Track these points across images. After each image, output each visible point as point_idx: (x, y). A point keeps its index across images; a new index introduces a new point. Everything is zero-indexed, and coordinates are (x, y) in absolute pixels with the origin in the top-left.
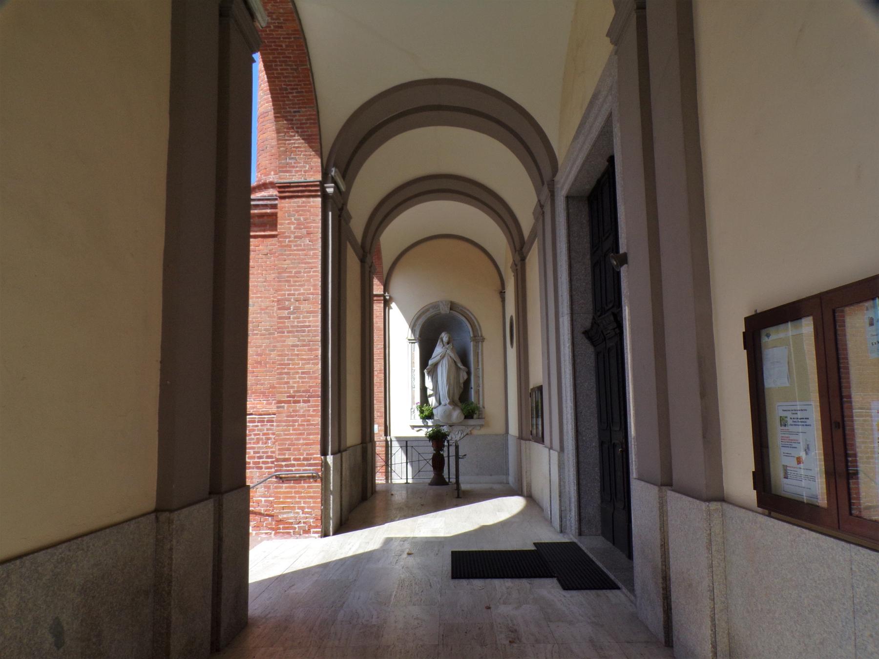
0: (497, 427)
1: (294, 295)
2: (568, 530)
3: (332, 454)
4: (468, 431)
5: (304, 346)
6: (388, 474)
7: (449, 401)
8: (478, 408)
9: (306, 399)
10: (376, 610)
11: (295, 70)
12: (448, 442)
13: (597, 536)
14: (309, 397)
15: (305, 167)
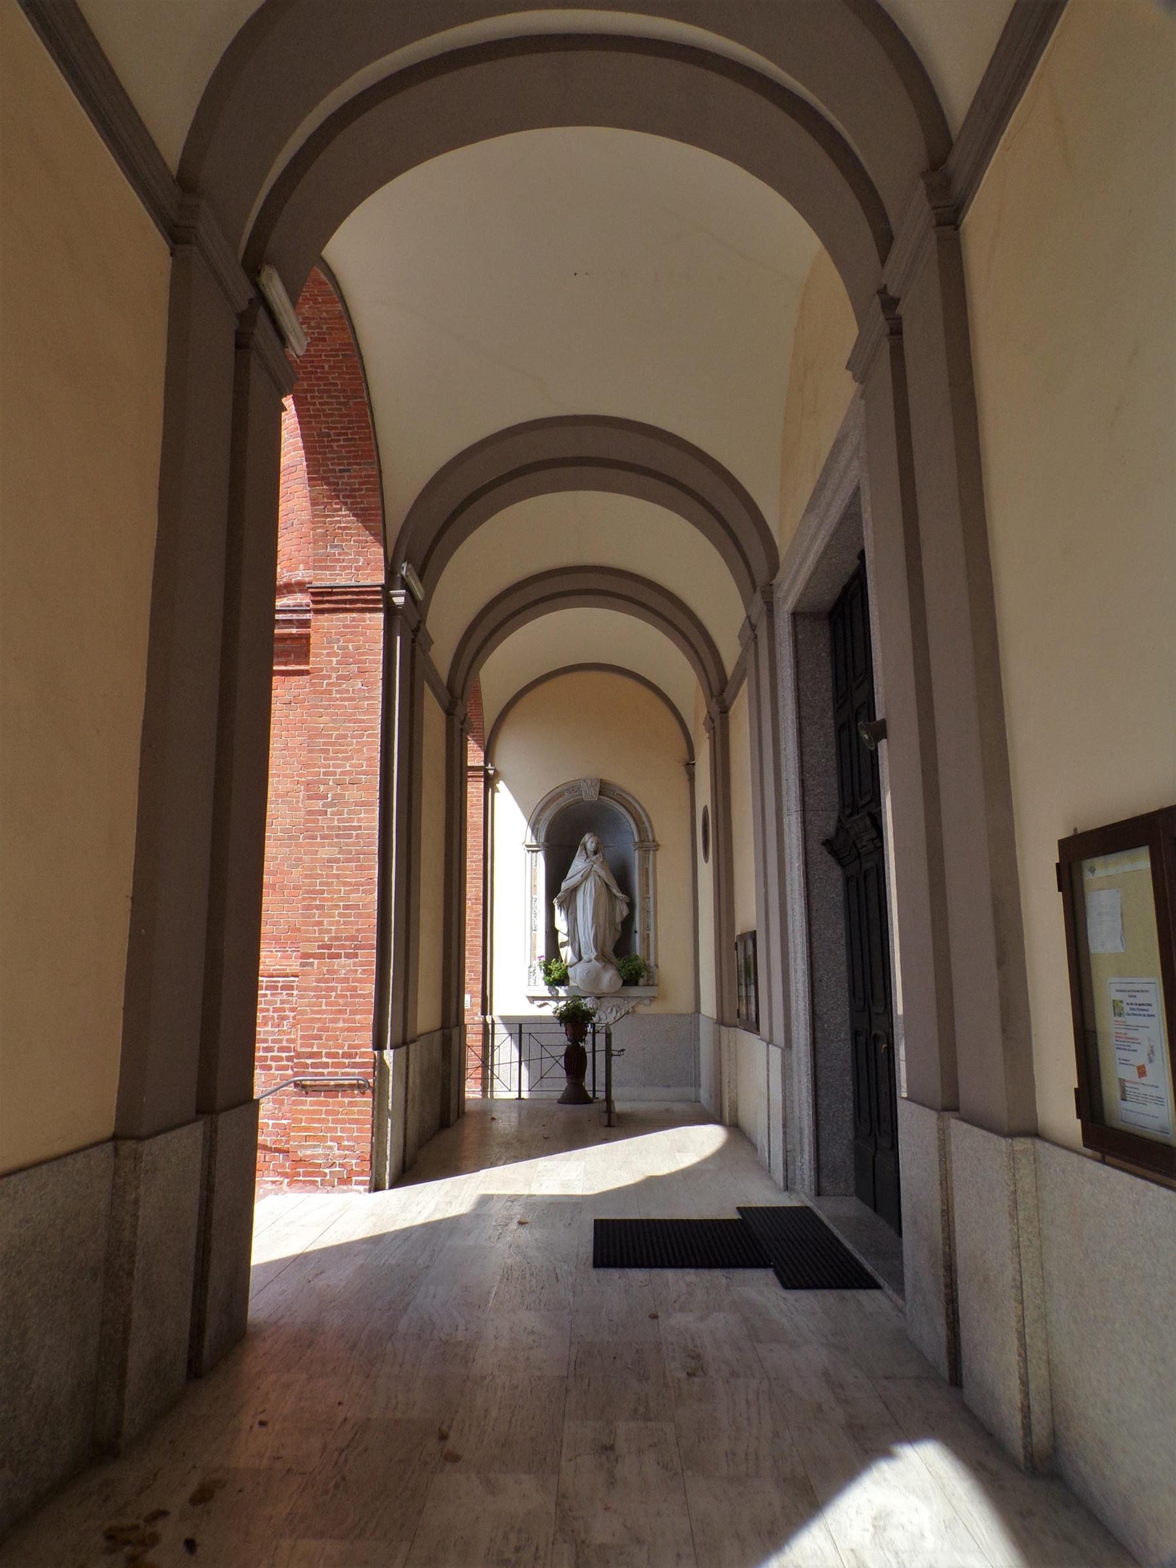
0: (680, 1003)
1: (334, 774)
2: (798, 1187)
3: (391, 1048)
4: (628, 1006)
5: (348, 860)
6: (486, 1082)
7: (595, 954)
8: (647, 968)
9: (351, 951)
10: (464, 1317)
11: (344, 404)
12: (594, 1026)
13: (847, 1196)
14: (356, 948)
15: (357, 561)
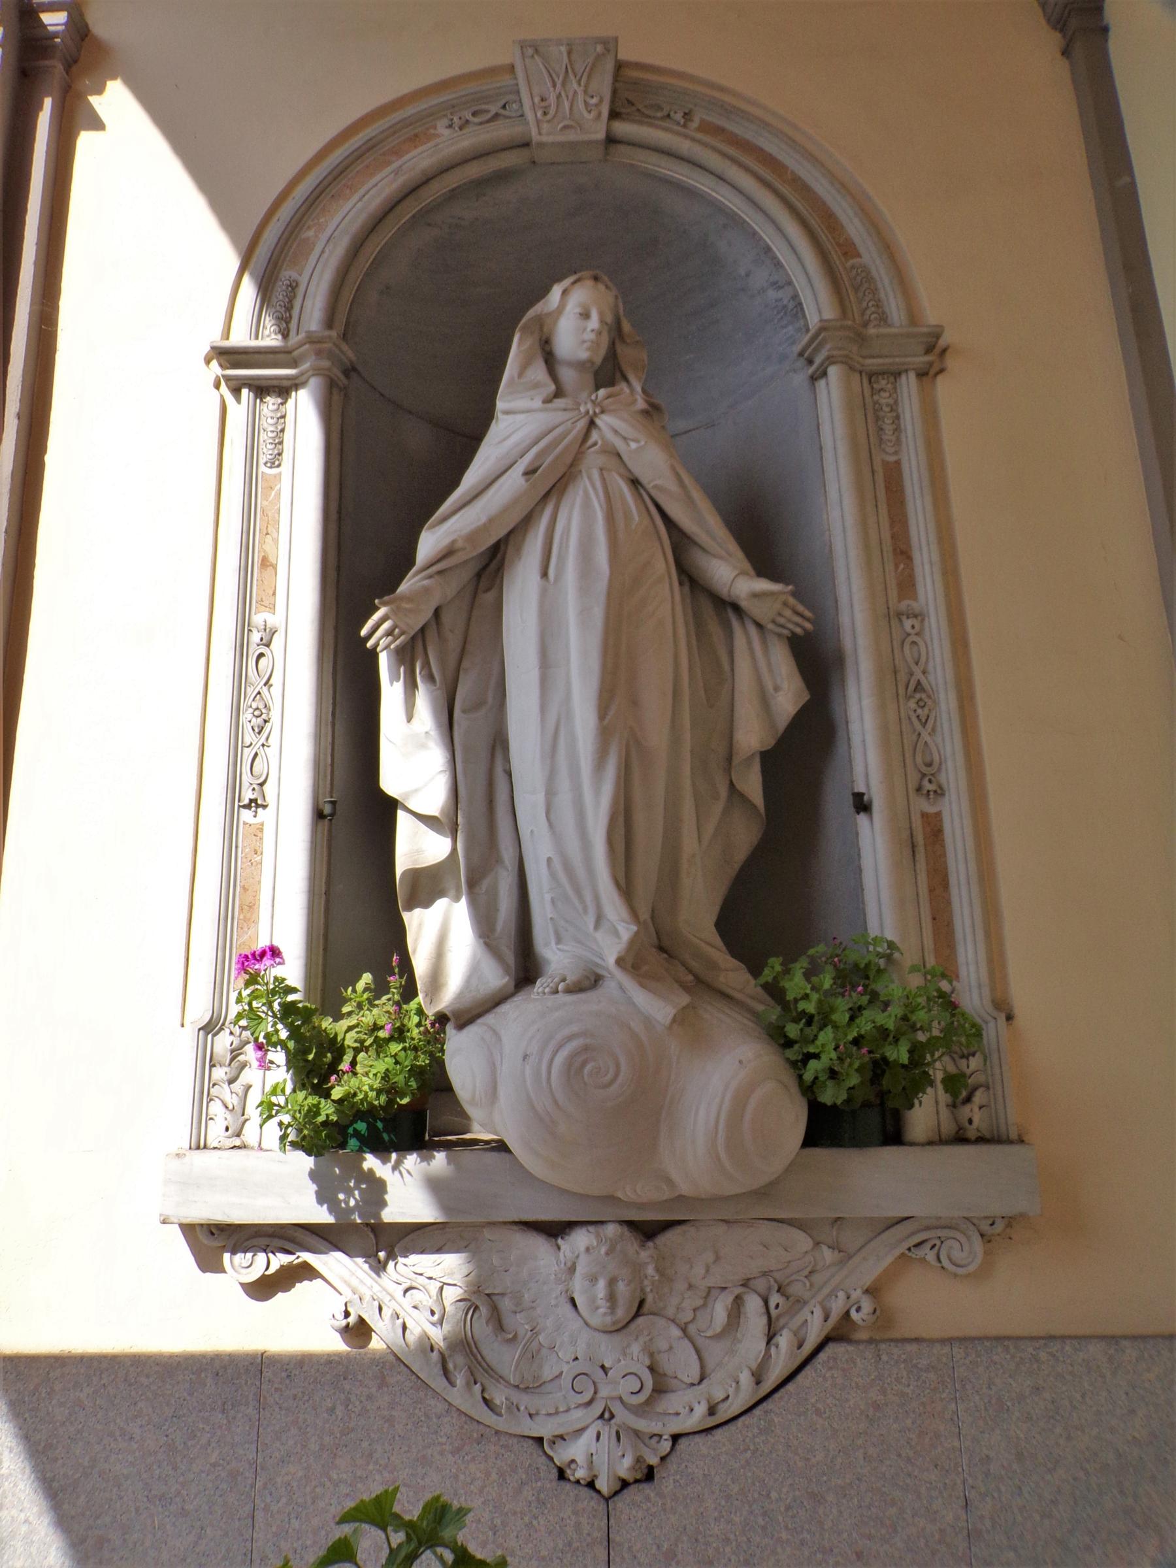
7: (626, 931)
